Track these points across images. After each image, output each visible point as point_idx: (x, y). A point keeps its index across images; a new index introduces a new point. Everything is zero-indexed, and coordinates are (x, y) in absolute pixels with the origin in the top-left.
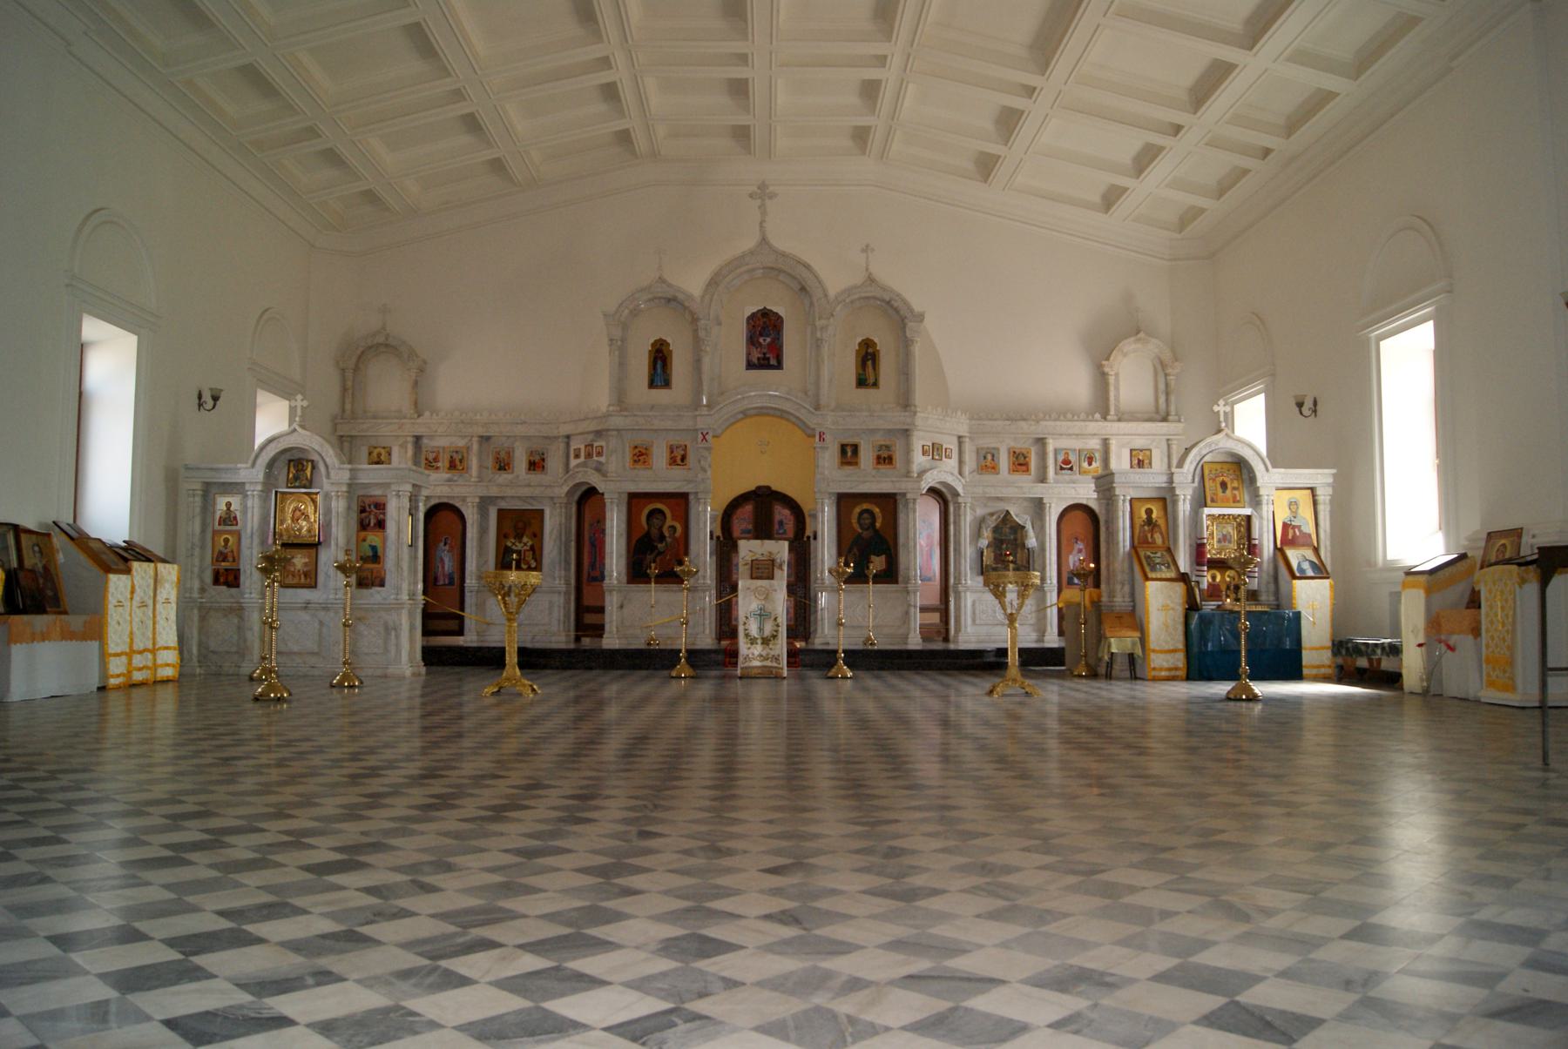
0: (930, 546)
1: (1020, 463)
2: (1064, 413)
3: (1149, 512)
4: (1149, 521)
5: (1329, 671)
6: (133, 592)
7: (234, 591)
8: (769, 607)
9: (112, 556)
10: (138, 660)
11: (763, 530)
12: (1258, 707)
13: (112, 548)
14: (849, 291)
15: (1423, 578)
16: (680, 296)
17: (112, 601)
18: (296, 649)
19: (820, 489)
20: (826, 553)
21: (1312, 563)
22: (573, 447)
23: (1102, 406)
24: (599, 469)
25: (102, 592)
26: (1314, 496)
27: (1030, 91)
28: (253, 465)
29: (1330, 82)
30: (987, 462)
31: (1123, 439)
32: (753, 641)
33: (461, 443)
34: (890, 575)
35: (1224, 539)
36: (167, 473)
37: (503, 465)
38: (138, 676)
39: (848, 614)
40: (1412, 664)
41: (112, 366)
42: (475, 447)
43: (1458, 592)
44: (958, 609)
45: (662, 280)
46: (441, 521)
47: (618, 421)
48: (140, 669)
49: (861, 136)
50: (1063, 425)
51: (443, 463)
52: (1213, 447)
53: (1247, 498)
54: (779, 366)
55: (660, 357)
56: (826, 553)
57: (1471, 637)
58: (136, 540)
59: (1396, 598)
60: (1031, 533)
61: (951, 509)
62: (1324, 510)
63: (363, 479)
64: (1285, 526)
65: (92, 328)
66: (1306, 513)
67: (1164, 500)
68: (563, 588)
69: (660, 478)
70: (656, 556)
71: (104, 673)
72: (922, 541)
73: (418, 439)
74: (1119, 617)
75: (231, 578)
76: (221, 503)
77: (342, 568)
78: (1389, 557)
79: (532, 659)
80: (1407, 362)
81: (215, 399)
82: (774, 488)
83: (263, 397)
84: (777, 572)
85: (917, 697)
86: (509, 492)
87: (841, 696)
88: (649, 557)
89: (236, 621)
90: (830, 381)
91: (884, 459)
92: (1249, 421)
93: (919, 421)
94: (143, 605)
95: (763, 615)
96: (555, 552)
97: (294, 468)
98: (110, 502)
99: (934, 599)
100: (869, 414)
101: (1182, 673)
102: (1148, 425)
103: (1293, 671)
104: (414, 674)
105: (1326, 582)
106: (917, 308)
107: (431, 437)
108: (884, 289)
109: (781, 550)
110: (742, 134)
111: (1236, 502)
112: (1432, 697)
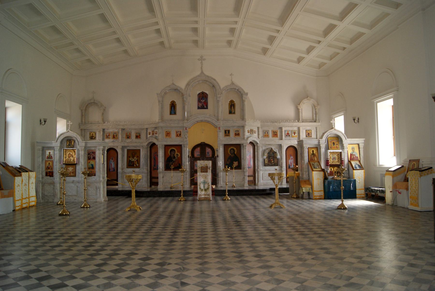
0: (250, 158)
1: (275, 134)
2: (287, 120)
3: (313, 151)
4: (313, 154)
5: (363, 196)
6: (22, 182)
7: (52, 178)
8: (206, 180)
9: (16, 171)
10: (24, 201)
11: (203, 157)
12: (346, 211)
13: (16, 168)
14: (226, 87)
15: (392, 173)
16: (179, 88)
17: (16, 185)
18: (70, 194)
19: (219, 143)
20: (221, 163)
21: (358, 165)
23: (298, 118)
24: (156, 138)
25: (13, 182)
26: (359, 146)
27: (278, 31)
28: (57, 141)
29: (363, 30)
30: (266, 134)
31: (304, 127)
32: (202, 190)
33: (116, 131)
34: (239, 167)
35: (334, 158)
36: (31, 144)
37: (128, 137)
38: (24, 206)
39: (229, 179)
40: (389, 196)
41: (14, 114)
42: (120, 132)
43: (401, 177)
44: (258, 176)
45: (173, 84)
46: (111, 153)
47: (161, 125)
48: (25, 204)
49: (229, 43)
50: (286, 124)
51: (111, 136)
52: (330, 133)
53: (340, 147)
54: (207, 108)
55: (173, 106)
56: (221, 163)
57: (406, 190)
58: (23, 165)
59: (383, 176)
60: (278, 154)
62: (362, 150)
63: (89, 145)
64: (351, 155)
65: (8, 103)
66: (357, 151)
67: (317, 148)
68: (146, 172)
69: (174, 140)
71: (14, 206)
72: (248, 157)
73: (104, 130)
74: (305, 181)
75: (51, 174)
76: (47, 152)
77: (83, 173)
78: (380, 164)
79: (140, 194)
80: (385, 109)
81: (45, 122)
83: (59, 119)
84: (208, 170)
85: (248, 203)
86: (130, 145)
87: (227, 205)
88: (171, 163)
89: (52, 186)
91: (237, 134)
92: (339, 124)
94: (26, 185)
95: (204, 183)
96: (144, 161)
97: (68, 142)
98: (15, 154)
99: (251, 173)
100: (232, 122)
101: (323, 197)
102: (311, 123)
103: (352, 195)
104: (104, 200)
105: (363, 171)
106: (246, 91)
107: (107, 129)
109: (209, 163)
110: (196, 42)
111: (337, 148)
112: (394, 206)
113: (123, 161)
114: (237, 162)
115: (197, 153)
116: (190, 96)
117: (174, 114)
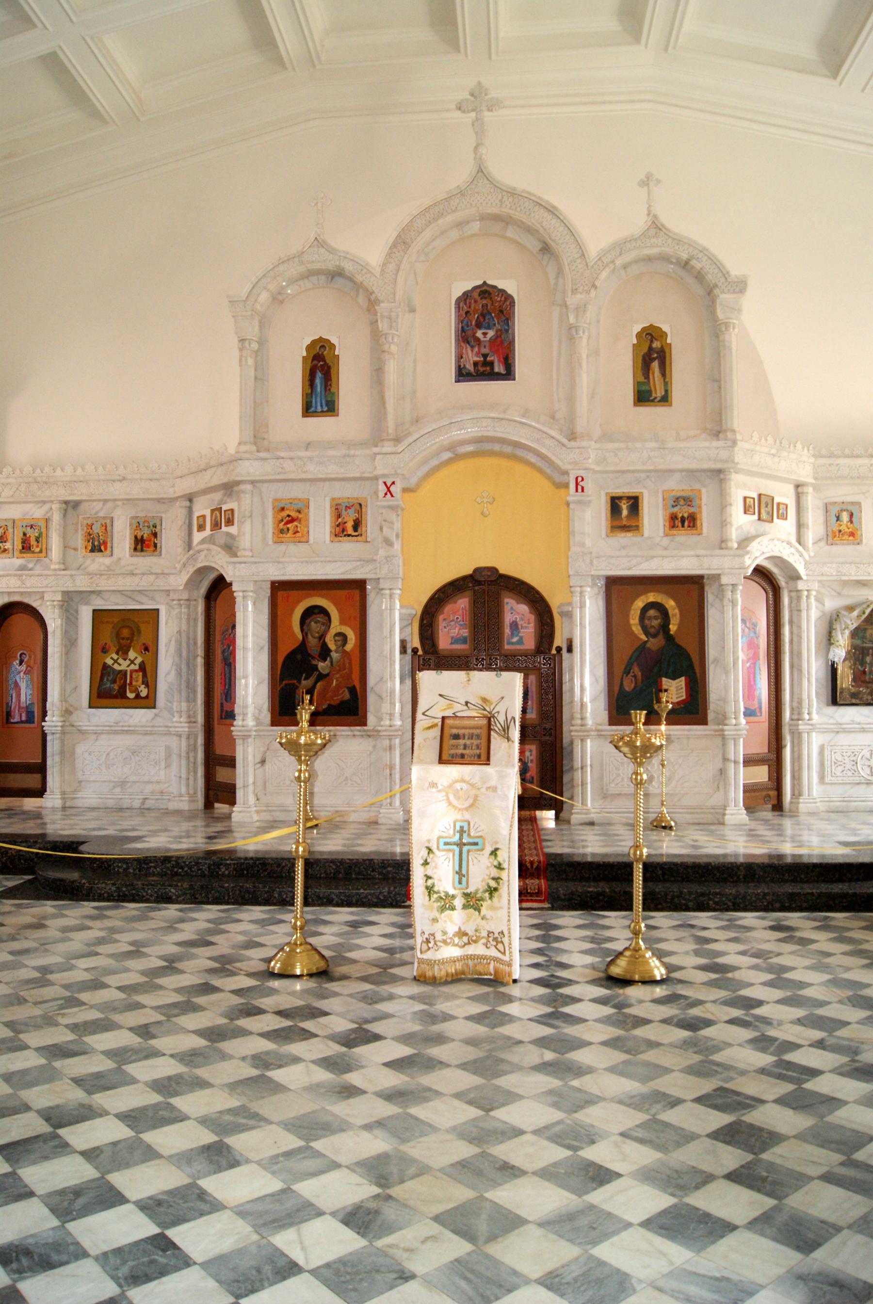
8: (479, 827)
11: (485, 650)
14: (621, 246)
16: (348, 267)
19: (580, 580)
20: (587, 682)
22: (196, 514)
24: (230, 548)
33: (38, 513)
34: (693, 710)
37: (98, 545)
42: (56, 518)
44: (797, 759)
47: (250, 469)
54: (509, 374)
55: (320, 367)
56: (587, 682)
61: (785, 600)
68: (184, 728)
69: (322, 557)
70: (319, 681)
82: (503, 570)
86: (104, 584)
88: (306, 683)
90: (592, 396)
91: (683, 519)
93: (740, 457)
99: (761, 747)
100: (654, 450)
106: (735, 270)
108: (679, 241)
109: (505, 692)
113: (68, 668)
114: (682, 681)
115: (452, 630)
116: (412, 310)
117: (322, 414)
